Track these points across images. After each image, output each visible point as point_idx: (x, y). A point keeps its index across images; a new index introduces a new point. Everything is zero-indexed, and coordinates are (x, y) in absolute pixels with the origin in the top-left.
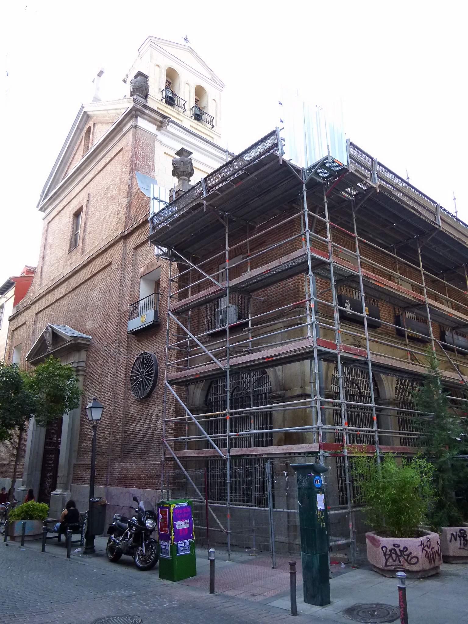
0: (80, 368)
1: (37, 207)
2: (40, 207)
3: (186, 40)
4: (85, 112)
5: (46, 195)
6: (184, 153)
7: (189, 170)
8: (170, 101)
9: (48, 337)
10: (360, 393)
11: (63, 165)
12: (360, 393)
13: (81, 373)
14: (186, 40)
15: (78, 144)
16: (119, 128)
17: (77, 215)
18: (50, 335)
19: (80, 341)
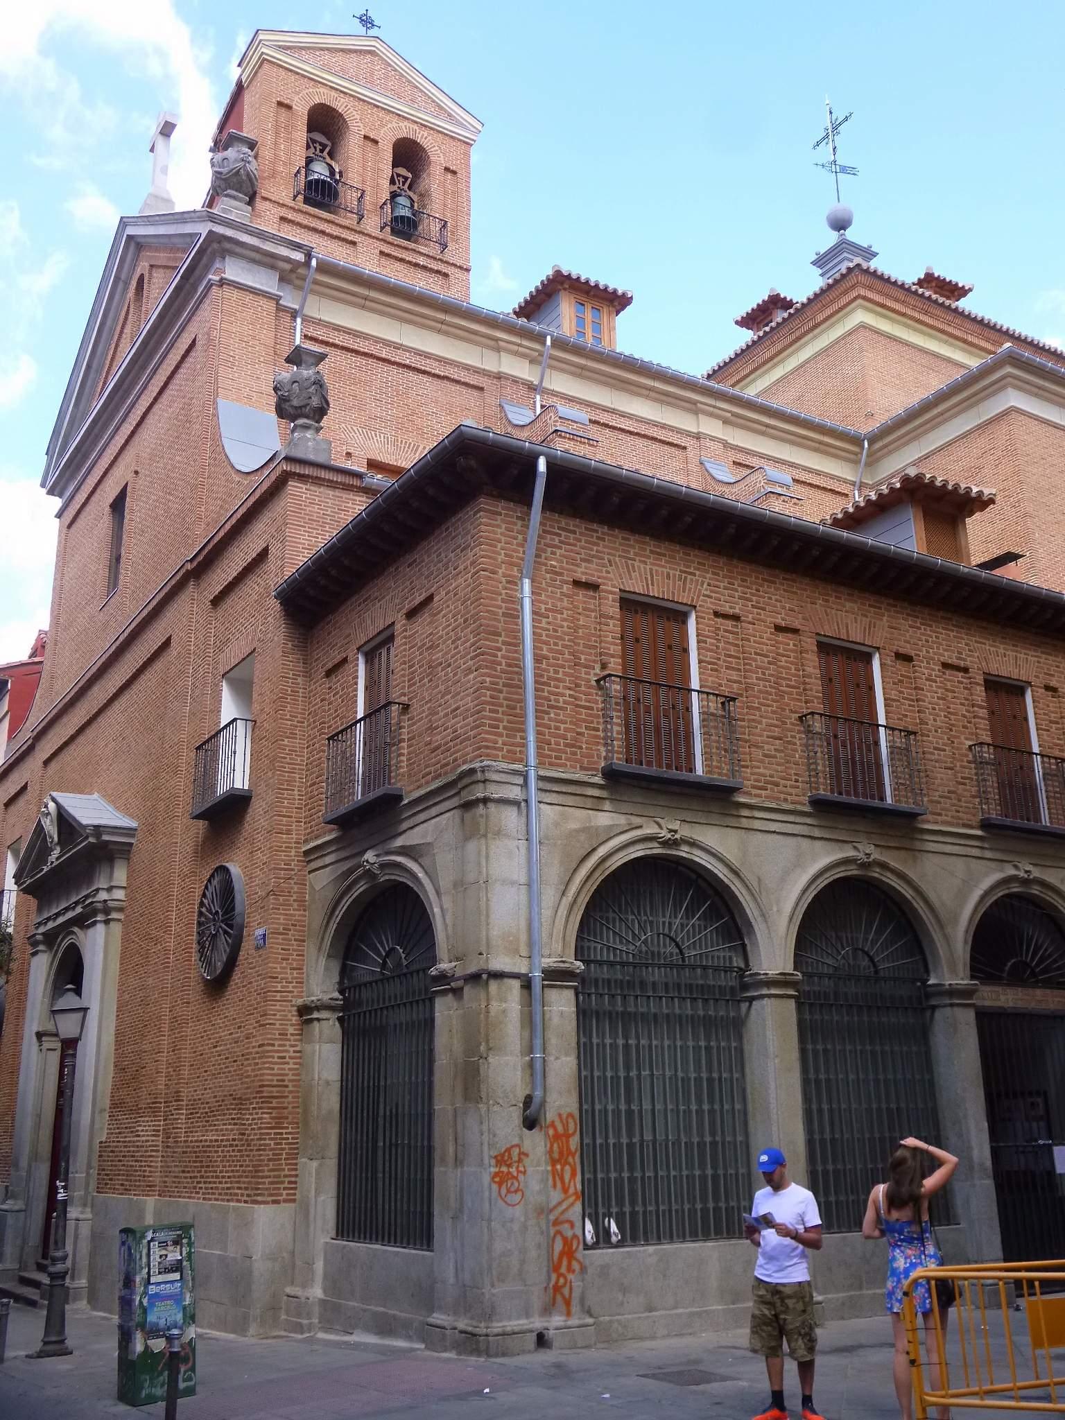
0: (111, 904)
1: (43, 485)
2: (49, 484)
3: (366, 21)
4: (130, 237)
5: (61, 455)
6: (304, 357)
7: (315, 402)
8: (321, 194)
9: (51, 827)
10: (876, 972)
11: (92, 375)
12: (876, 972)
13: (114, 915)
14: (366, 21)
15: (123, 313)
16: (188, 286)
17: (118, 505)
18: (52, 821)
19: (105, 838)
